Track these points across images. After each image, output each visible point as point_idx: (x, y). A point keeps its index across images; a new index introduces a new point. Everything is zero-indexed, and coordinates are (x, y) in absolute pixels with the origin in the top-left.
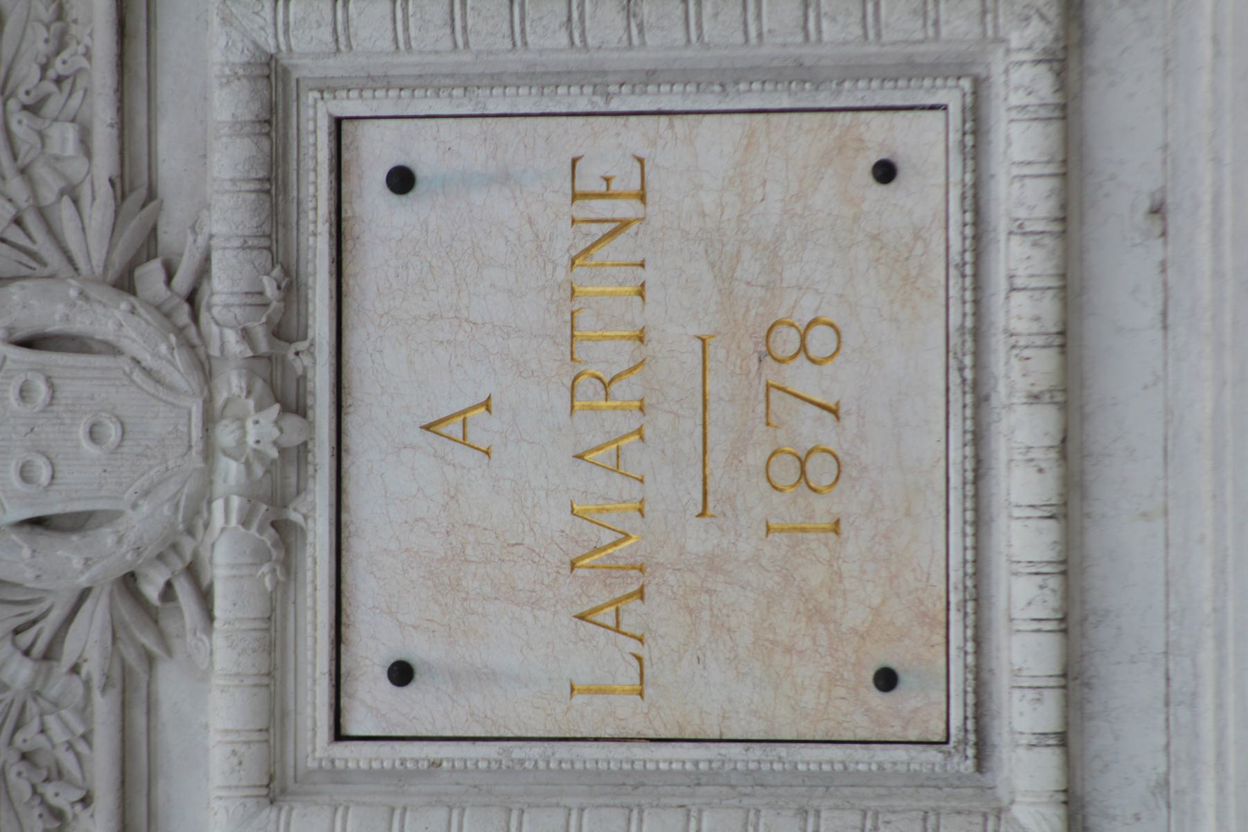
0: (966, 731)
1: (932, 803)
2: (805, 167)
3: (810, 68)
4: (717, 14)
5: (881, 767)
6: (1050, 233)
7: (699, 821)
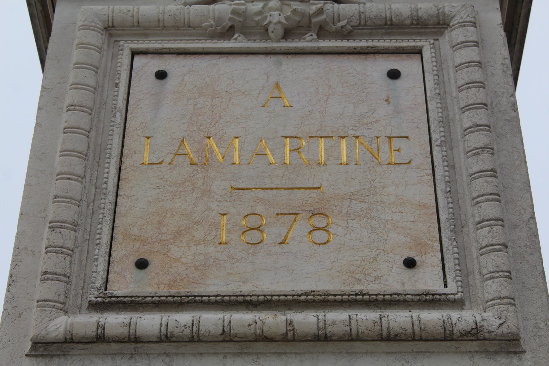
0: (111, 297)
1: (74, 281)
2: (410, 229)
3: (462, 231)
4: (487, 182)
5: (96, 259)
6: (381, 330)
7: (76, 180)
